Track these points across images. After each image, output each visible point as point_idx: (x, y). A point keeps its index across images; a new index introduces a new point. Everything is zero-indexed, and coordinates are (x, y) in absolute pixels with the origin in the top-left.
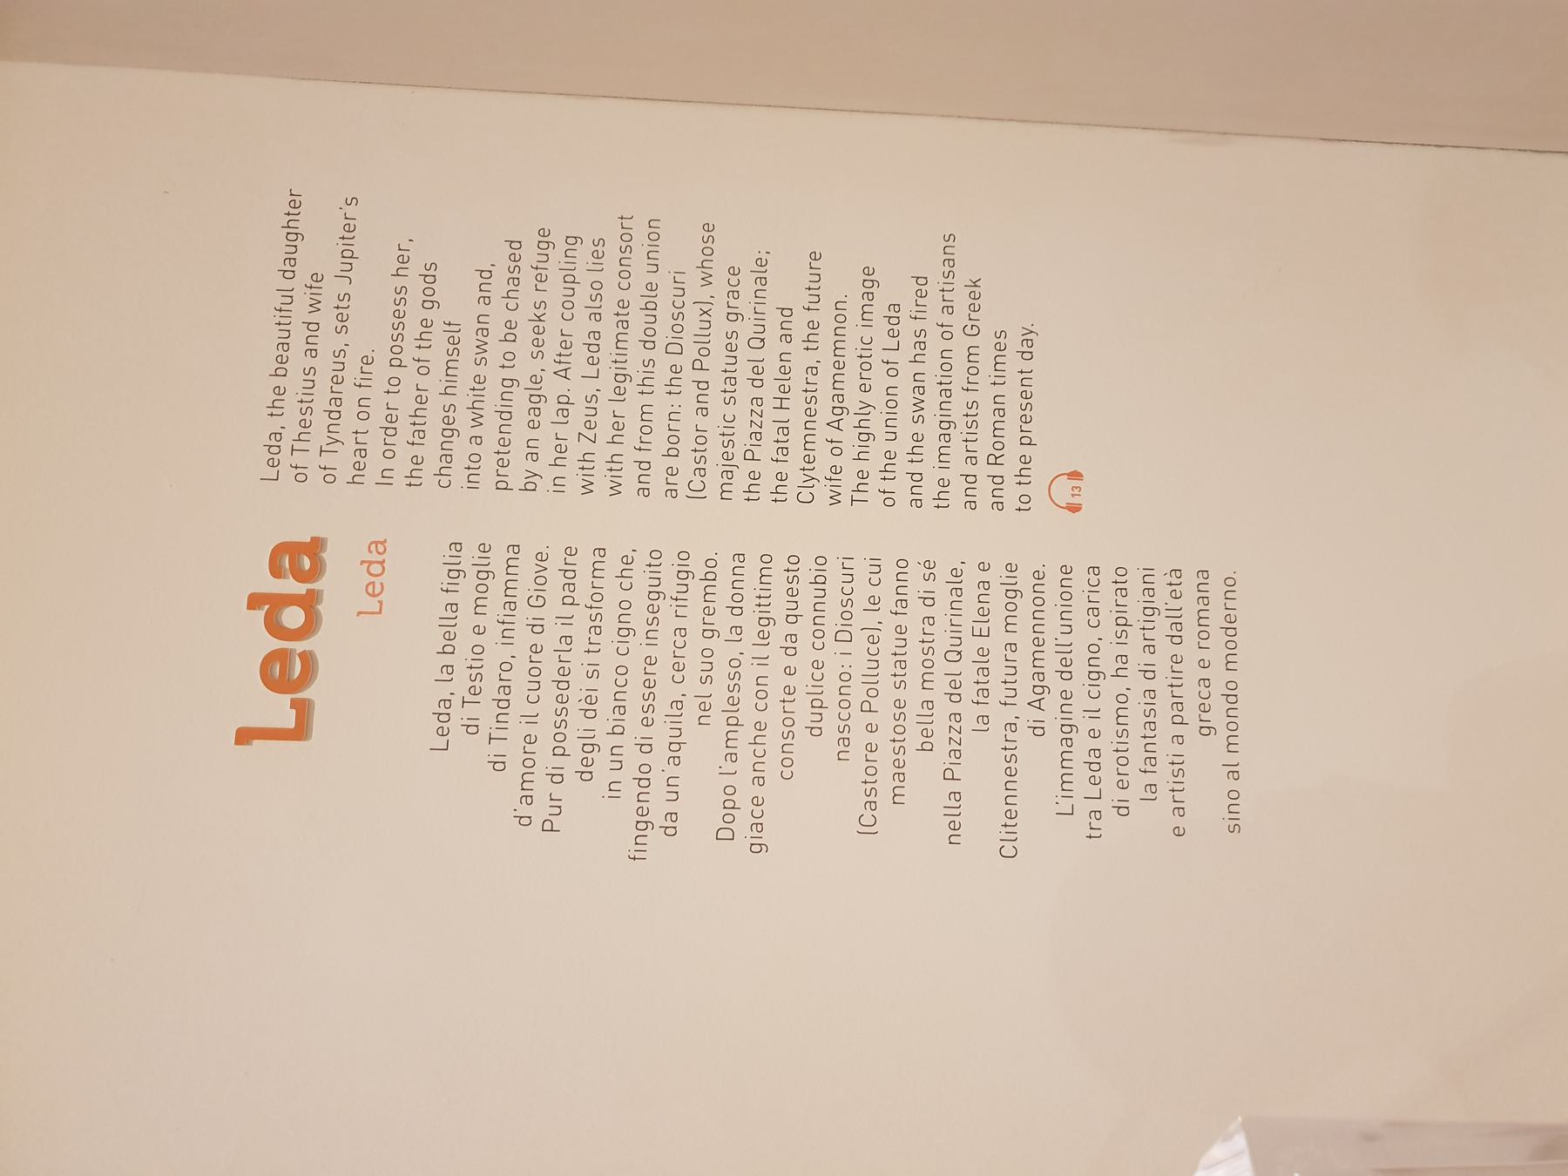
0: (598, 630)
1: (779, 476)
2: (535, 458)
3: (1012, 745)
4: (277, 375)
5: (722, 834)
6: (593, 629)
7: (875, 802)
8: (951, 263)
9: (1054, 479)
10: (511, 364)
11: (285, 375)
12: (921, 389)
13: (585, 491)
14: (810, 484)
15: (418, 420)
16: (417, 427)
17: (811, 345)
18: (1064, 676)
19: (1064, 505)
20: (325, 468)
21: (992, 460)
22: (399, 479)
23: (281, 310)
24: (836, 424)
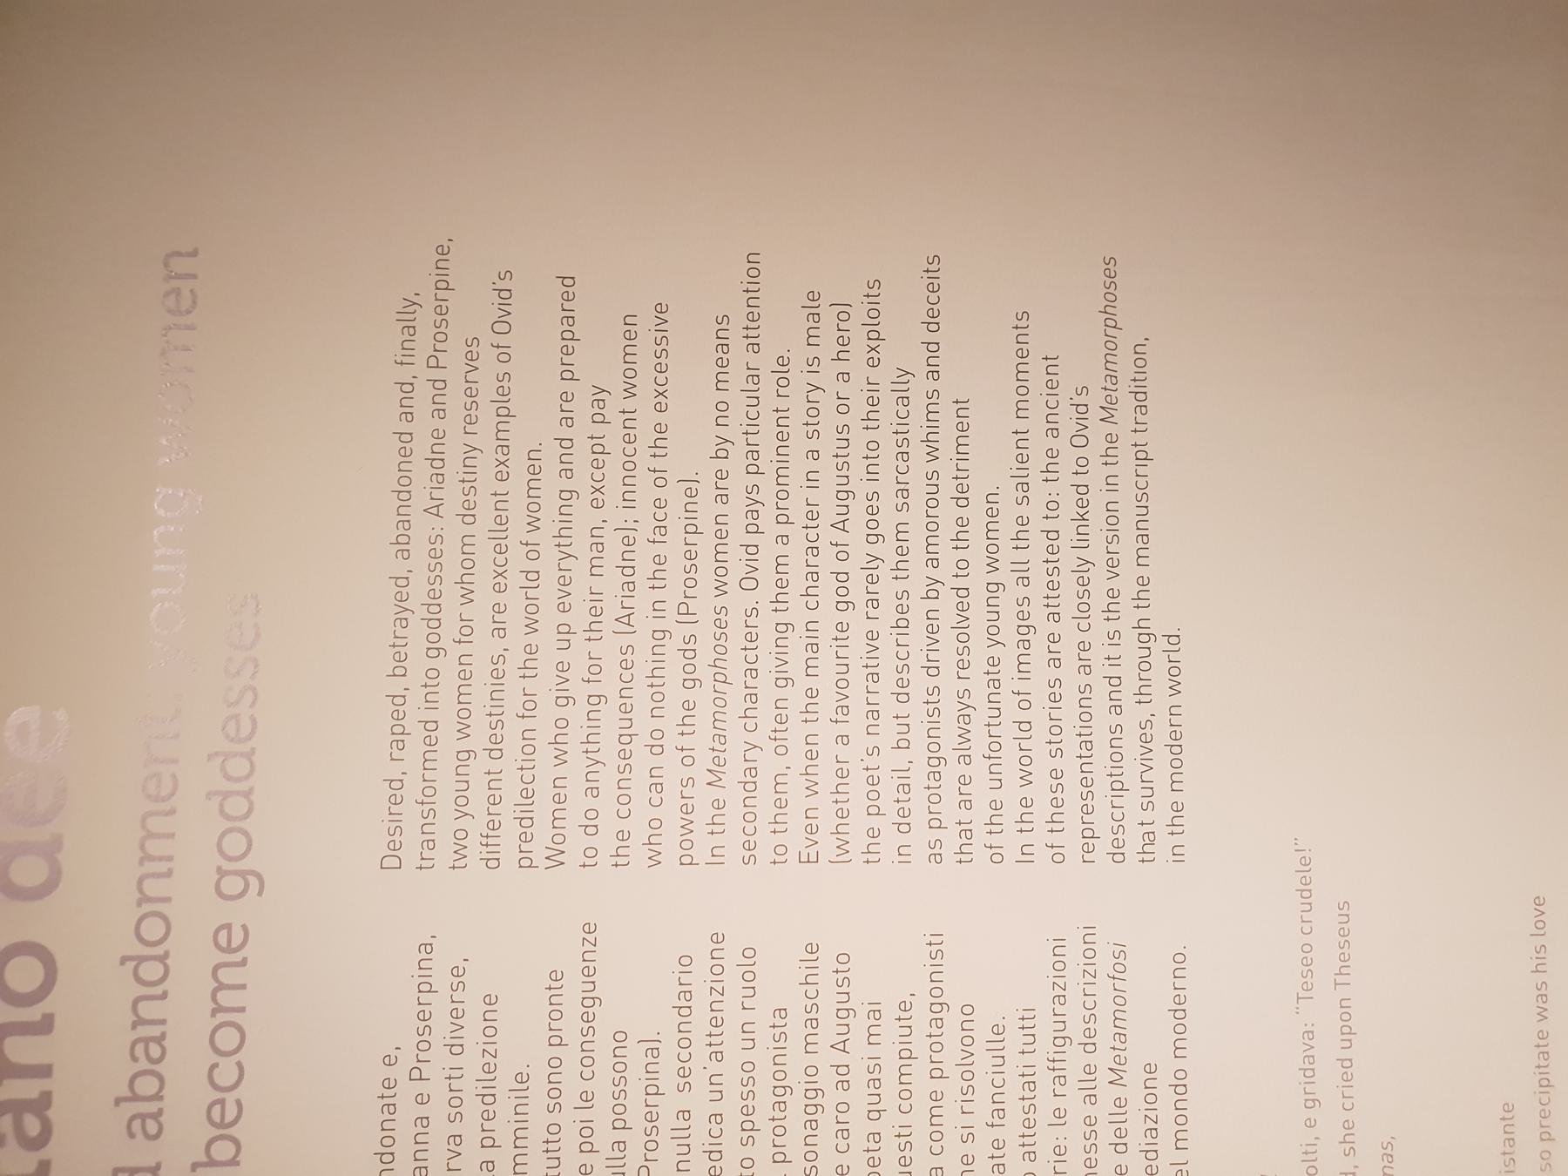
3: (964, 474)
4: (395, 675)
5: (387, 862)
10: (782, 859)
11: (404, 675)
12: (875, 714)
14: (1084, 568)
16: (714, 1049)
22: (604, 859)
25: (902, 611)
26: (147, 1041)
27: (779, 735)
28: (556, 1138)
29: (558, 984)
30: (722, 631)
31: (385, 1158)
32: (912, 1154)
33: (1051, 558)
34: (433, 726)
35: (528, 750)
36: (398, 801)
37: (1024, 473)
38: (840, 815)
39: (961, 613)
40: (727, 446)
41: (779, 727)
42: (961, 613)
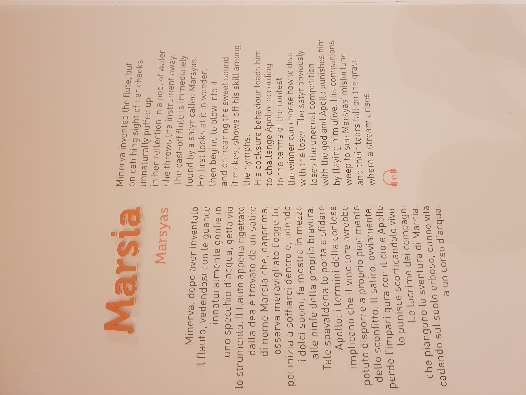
8: (303, 101)
9: (386, 172)
13: (161, 70)
15: (325, 174)
16: (194, 215)
17: (212, 184)
19: (390, 184)
24: (323, 113)
26: (162, 246)
28: (277, 214)
34: (126, 118)
35: (158, 127)
36: (323, 209)
37: (353, 346)
38: (276, 300)
40: (166, 229)
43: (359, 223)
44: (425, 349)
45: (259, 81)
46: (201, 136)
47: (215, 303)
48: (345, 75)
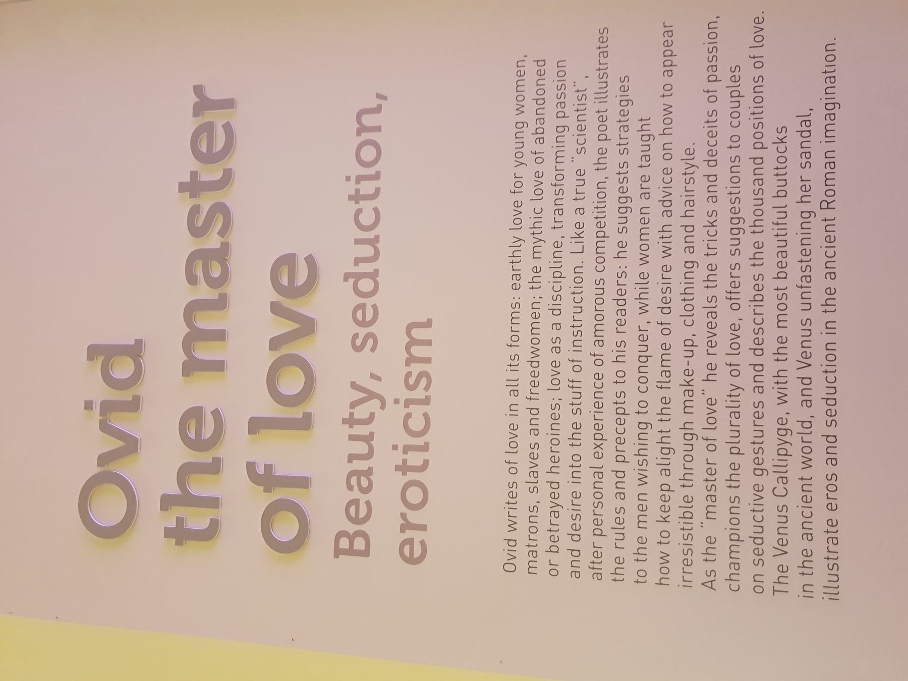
0: (558, 350)
1: (556, 244)
2: (558, 351)
6: (557, 211)
7: (559, 347)
17: (600, 167)
18: (664, 311)
20: (535, 153)
21: (824, 205)
23: (777, 224)
25: (758, 289)
27: (596, 566)
29: (834, 529)
30: (760, 557)
31: (620, 302)
32: (764, 456)
33: (710, 478)
39: (710, 407)
41: (596, 560)
42: (710, 407)
43: (557, 460)
44: (551, 434)
45: (714, 321)
46: (708, 221)
47: (532, 549)
48: (580, 144)
